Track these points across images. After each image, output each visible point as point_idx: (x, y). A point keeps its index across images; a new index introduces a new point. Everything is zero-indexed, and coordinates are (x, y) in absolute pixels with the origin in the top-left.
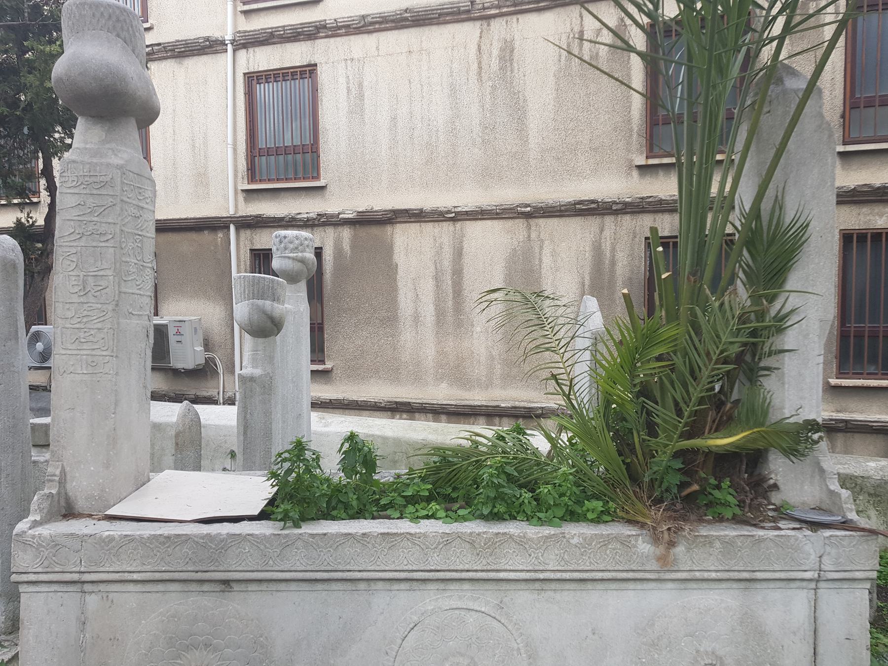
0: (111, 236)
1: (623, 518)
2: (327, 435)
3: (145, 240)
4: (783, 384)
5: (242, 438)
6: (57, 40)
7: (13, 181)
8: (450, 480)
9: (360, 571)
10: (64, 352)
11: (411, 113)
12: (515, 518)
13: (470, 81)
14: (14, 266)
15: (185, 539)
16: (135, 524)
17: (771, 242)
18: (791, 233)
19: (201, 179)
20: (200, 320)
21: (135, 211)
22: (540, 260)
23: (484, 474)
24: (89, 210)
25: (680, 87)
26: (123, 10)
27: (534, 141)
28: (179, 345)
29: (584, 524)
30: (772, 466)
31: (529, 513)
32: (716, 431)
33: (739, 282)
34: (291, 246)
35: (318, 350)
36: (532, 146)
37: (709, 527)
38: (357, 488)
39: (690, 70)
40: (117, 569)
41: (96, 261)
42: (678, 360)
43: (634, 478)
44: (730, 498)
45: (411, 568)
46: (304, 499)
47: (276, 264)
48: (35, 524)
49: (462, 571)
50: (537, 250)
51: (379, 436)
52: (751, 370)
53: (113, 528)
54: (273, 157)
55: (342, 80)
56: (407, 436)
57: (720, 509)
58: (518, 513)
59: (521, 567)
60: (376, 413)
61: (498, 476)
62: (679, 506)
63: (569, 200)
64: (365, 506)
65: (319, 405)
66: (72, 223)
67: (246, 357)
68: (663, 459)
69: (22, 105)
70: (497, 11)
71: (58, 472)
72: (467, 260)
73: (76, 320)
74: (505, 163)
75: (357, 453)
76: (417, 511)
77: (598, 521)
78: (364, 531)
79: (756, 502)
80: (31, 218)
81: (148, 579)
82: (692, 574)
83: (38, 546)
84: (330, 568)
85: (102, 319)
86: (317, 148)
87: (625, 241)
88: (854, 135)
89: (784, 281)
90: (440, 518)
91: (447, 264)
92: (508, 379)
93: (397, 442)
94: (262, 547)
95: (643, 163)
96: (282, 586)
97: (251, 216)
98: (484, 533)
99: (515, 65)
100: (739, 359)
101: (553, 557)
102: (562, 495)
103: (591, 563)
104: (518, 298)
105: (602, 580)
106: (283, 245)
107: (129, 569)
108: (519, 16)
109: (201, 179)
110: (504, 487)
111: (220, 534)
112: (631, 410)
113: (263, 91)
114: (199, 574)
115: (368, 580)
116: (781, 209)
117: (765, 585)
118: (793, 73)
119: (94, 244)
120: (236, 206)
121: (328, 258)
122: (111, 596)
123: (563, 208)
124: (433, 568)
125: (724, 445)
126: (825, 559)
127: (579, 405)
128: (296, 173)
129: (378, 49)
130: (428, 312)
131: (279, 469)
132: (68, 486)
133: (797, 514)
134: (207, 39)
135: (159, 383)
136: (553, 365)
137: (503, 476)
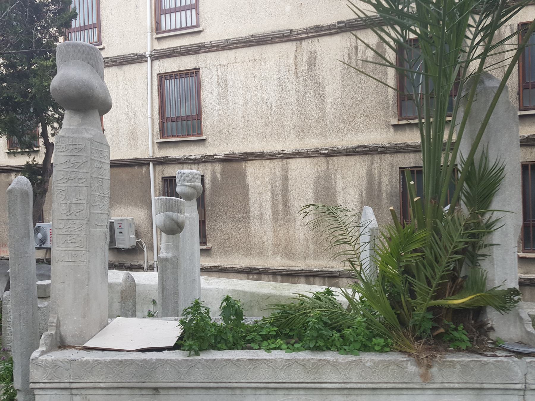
0: (85, 180)
1: (397, 349)
2: (210, 290)
3: (104, 181)
4: (493, 265)
5: (161, 295)
6: (50, 57)
7: (25, 140)
8: (288, 325)
9: (236, 383)
11: (256, 96)
12: (330, 349)
13: (291, 77)
14: (27, 194)
15: (130, 362)
16: (101, 352)
17: (481, 179)
18: (493, 173)
19: (133, 136)
20: (133, 219)
21: (99, 164)
22: (335, 182)
23: (309, 322)
24: (72, 165)
25: (420, 86)
27: (329, 111)
28: (121, 234)
29: (373, 353)
30: (489, 316)
31: (339, 346)
32: (453, 295)
33: (462, 202)
34: (188, 179)
35: (203, 237)
36: (328, 114)
37: (452, 355)
38: (231, 329)
39: (426, 77)
40: (92, 381)
41: (76, 195)
42: (427, 252)
43: (403, 324)
44: (464, 337)
45: (267, 381)
47: (179, 189)
48: (43, 353)
49: (299, 383)
50: (333, 176)
51: (241, 291)
52: (473, 256)
53: (88, 355)
55: (215, 77)
57: (458, 343)
58: (332, 346)
59: (335, 381)
61: (318, 324)
62: (432, 342)
63: (352, 146)
64: (237, 340)
65: (205, 270)
66: (62, 172)
67: (162, 248)
68: (420, 312)
69: (30, 95)
70: (306, 36)
71: (55, 321)
72: (290, 182)
73: (65, 230)
74: (312, 125)
76: (269, 345)
77: (382, 351)
79: (480, 338)
80: (35, 161)
81: (110, 386)
82: (443, 385)
83: (45, 366)
87: (387, 172)
88: (526, 105)
89: (490, 202)
90: (284, 349)
91: (279, 184)
92: (317, 254)
93: (252, 294)
94: (177, 367)
95: (396, 123)
96: (190, 392)
97: (162, 158)
98: (312, 359)
99: (317, 66)
100: (464, 251)
101: (355, 374)
102: (358, 335)
103: (379, 378)
104: (324, 210)
105: (387, 389)
106: (182, 178)
107: (98, 381)
108: (319, 38)
109: (133, 136)
110: (322, 330)
112: (399, 281)
113: (168, 84)
114: (140, 384)
116: (486, 159)
117: (490, 392)
118: (490, 77)
119: (75, 185)
121: (207, 182)
122: (88, 397)
123: (348, 151)
124: (281, 381)
125: (459, 304)
126: (529, 377)
127: (366, 277)
128: (188, 132)
129: (235, 58)
130: (268, 213)
133: (506, 346)
134: (136, 54)
136: (347, 252)
137: (321, 323)
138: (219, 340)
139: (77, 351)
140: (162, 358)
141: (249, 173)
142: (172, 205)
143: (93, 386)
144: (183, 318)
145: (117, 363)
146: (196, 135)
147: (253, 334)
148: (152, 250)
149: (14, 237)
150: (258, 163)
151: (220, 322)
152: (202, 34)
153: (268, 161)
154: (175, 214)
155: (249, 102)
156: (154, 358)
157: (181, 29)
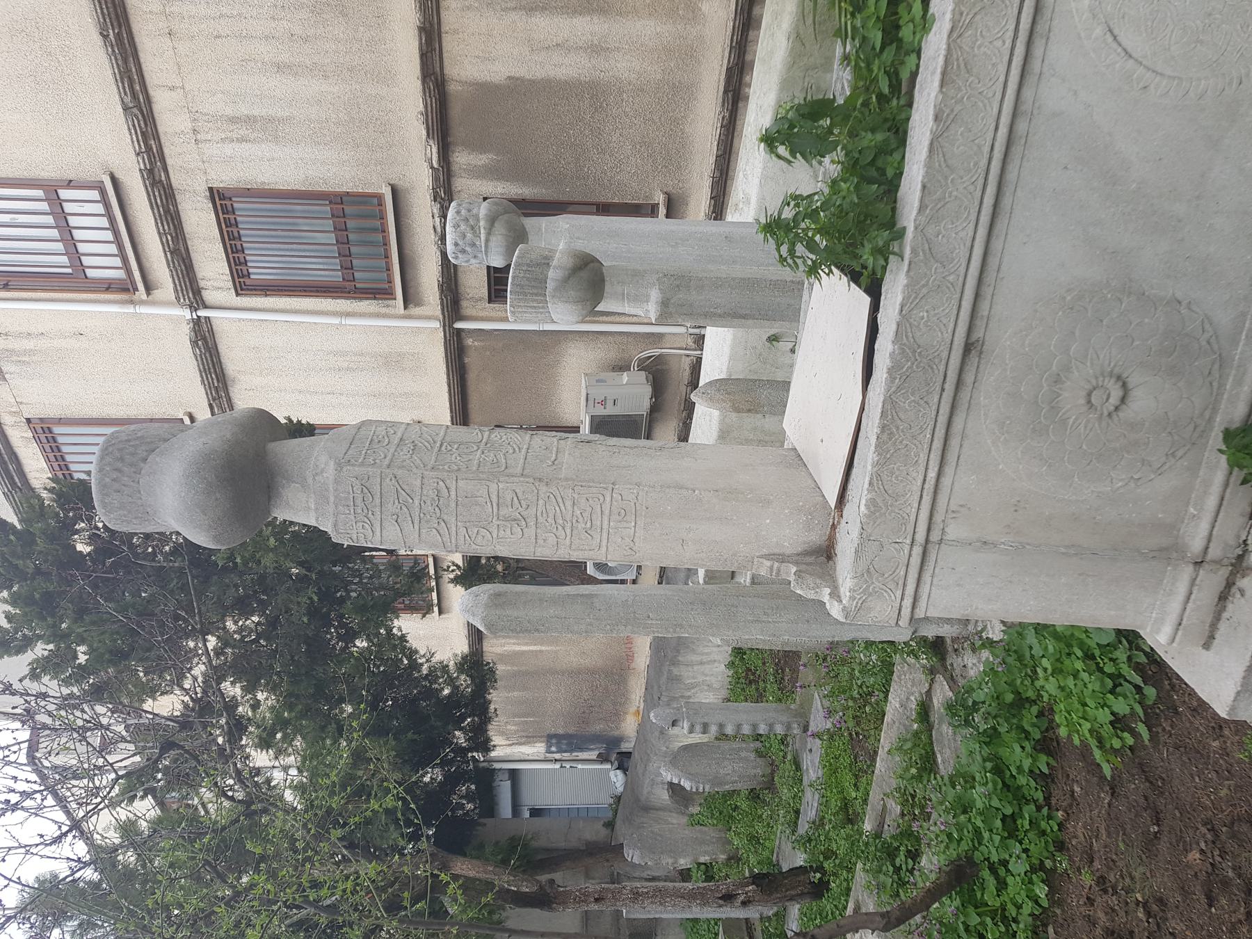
2: (762, 199)
3: (448, 439)
5: (750, 322)
9: (997, 128)
10: (604, 549)
11: (267, 37)
15: (890, 404)
16: (855, 471)
20: (586, 375)
26: (105, 451)
28: (619, 403)
34: (469, 235)
38: (853, 134)
45: (1010, 34)
46: (859, 222)
48: (835, 595)
53: (856, 500)
54: (354, 262)
55: (228, 149)
56: (779, 66)
60: (738, 128)
64: (886, 120)
65: (718, 208)
67: (636, 311)
71: (768, 563)
73: (561, 533)
75: (797, 132)
78: (931, 117)
81: (939, 458)
84: (981, 181)
85: (560, 500)
86: (336, 194)
94: (924, 291)
96: (993, 262)
106: (468, 249)
107: (919, 483)
109: (392, 362)
111: (892, 355)
113: (259, 270)
114: (947, 386)
115: (1015, 115)
119: (453, 505)
120: (429, 318)
122: (953, 507)
128: (375, 230)
130: (583, 27)
131: (804, 262)
132: (788, 552)
134: (194, 343)
135: (667, 431)
138: (876, 174)
139: (843, 522)
140: (894, 327)
141: (476, 75)
142: (528, 279)
143: (931, 494)
144: (802, 268)
145: (885, 437)
146: (381, 211)
147: (875, 69)
148: (661, 336)
149: (591, 624)
150: (451, 45)
151: (830, 166)
152: (119, 175)
153: (443, 14)
154: (551, 274)
155: (285, 57)
156: (890, 347)
157: (113, 228)
